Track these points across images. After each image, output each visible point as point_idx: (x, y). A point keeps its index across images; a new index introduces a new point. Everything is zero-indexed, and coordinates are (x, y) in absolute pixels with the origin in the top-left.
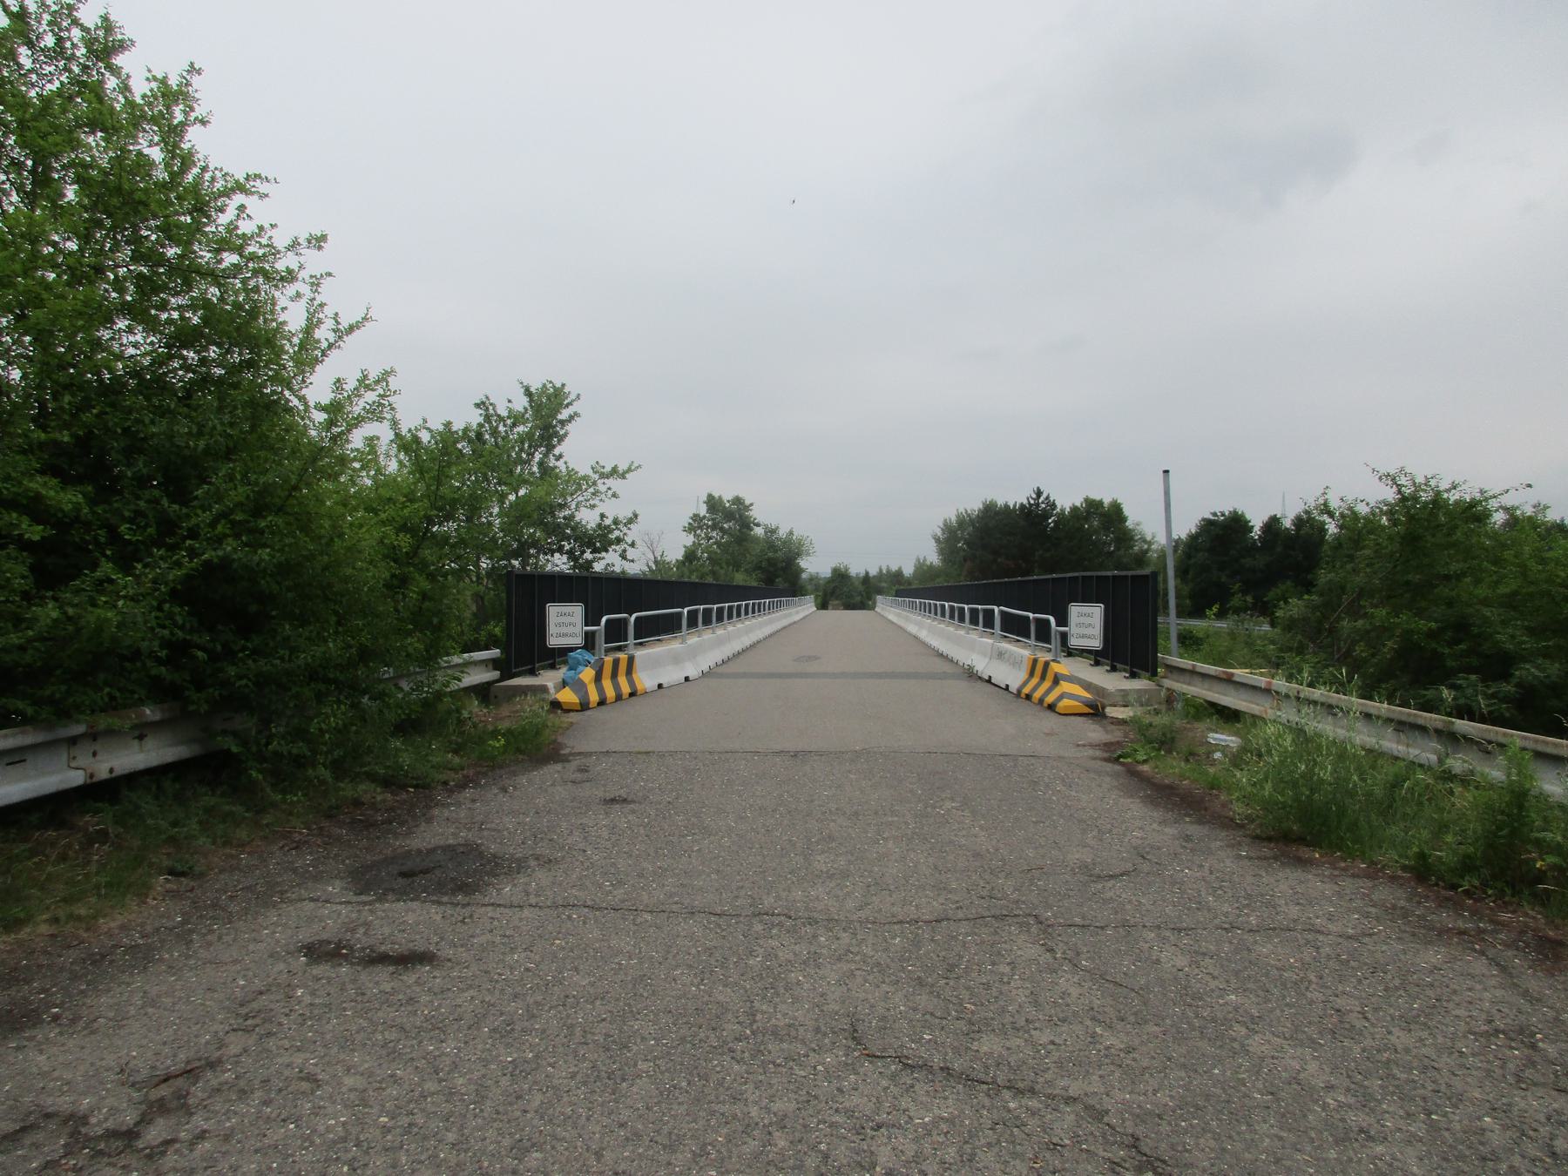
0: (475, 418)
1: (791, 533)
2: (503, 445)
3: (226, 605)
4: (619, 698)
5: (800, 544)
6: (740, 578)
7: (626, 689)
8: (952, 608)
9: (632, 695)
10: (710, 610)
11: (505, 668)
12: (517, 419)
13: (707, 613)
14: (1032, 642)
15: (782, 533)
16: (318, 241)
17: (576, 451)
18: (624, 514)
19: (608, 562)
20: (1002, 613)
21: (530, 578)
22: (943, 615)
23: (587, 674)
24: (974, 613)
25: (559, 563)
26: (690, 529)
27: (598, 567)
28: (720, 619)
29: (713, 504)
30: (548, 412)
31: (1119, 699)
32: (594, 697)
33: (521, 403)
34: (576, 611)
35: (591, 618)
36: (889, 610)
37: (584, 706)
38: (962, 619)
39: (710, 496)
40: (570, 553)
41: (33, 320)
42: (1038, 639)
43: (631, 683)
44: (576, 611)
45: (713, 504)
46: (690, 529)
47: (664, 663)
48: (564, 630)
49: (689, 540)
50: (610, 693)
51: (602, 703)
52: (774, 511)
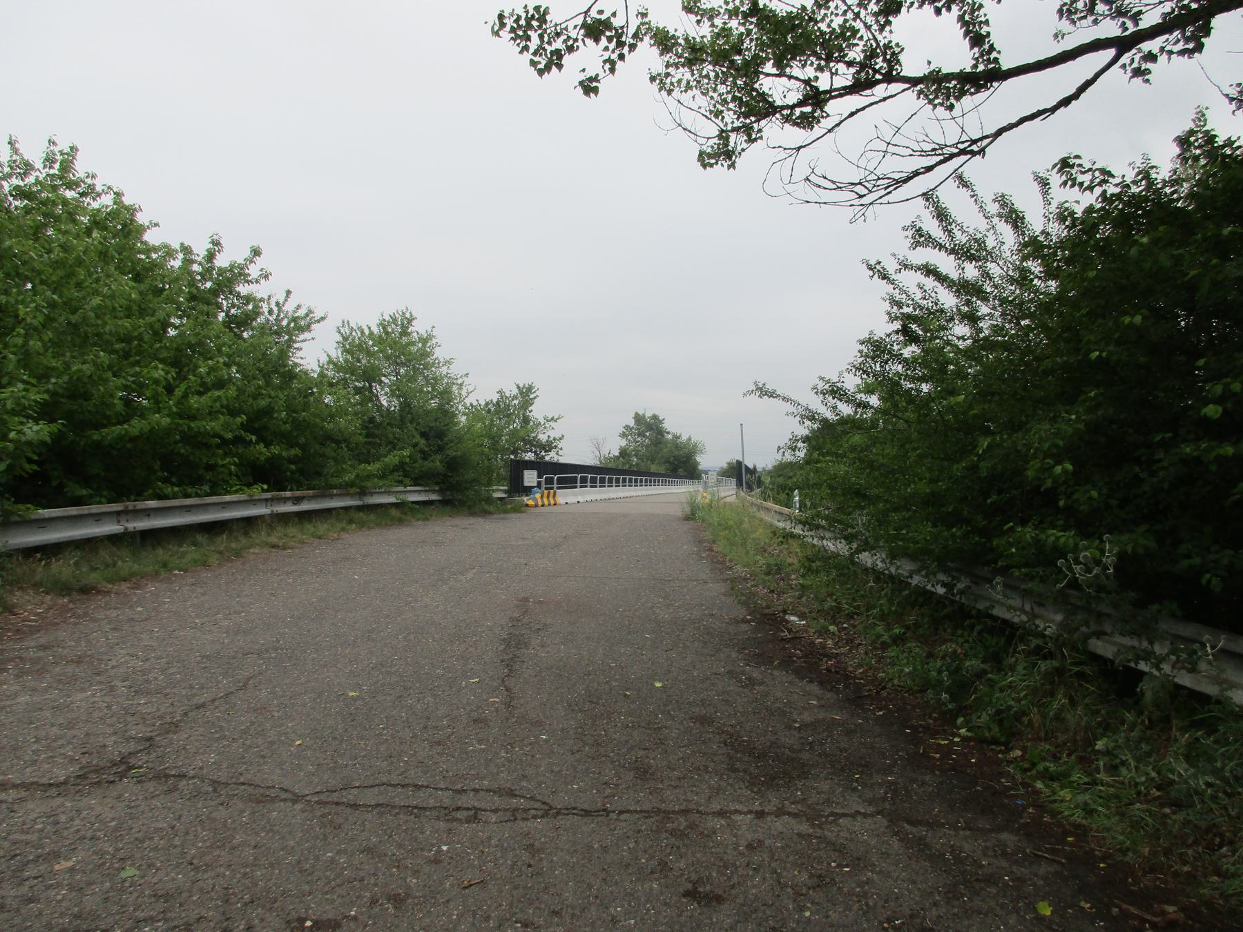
0: (495, 398)
1: (689, 439)
2: (508, 407)
3: (453, 465)
5: (695, 446)
6: (654, 468)
11: (509, 492)
12: (515, 397)
15: (684, 438)
17: (537, 412)
18: (558, 436)
19: (551, 457)
21: (518, 462)
23: (538, 496)
25: (530, 456)
26: (623, 435)
27: (547, 458)
29: (639, 419)
30: (526, 394)
32: (540, 503)
33: (515, 391)
34: (535, 473)
35: (540, 476)
37: (536, 506)
39: (637, 415)
40: (535, 453)
41: (1175, 732)
44: (535, 473)
45: (639, 419)
46: (623, 435)
47: (567, 497)
49: (624, 443)
52: (677, 426)
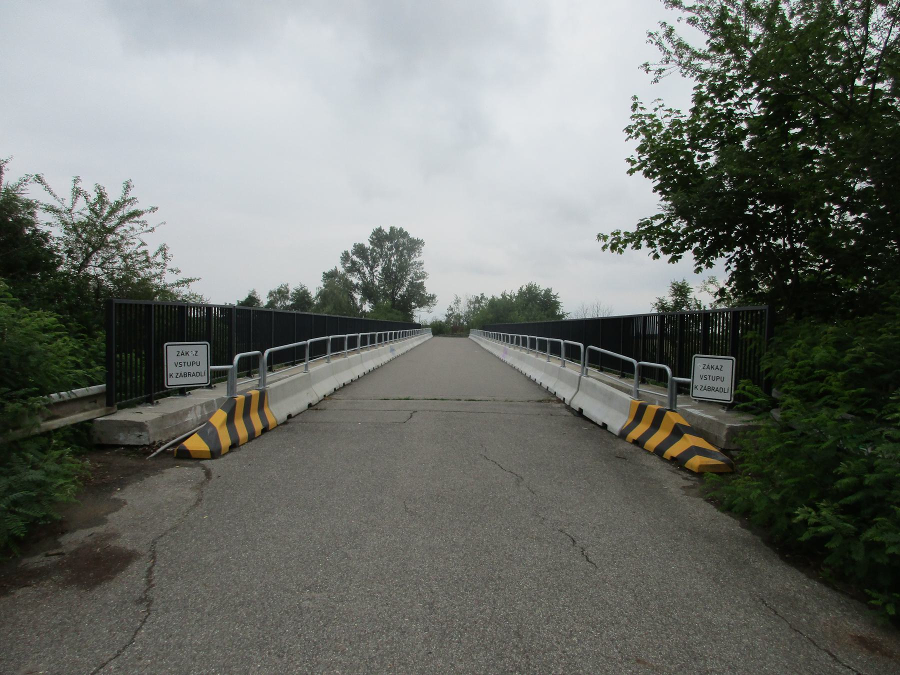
4: (252, 437)
7: (258, 426)
8: (512, 337)
9: (265, 430)
10: (374, 335)
13: (372, 337)
14: (548, 354)
16: (154, 209)
20: (566, 345)
22: (512, 342)
24: (533, 341)
28: (380, 340)
31: (209, 456)
32: (225, 441)
36: (475, 336)
38: (518, 343)
42: (540, 349)
43: (263, 417)
48: (709, 383)
50: (242, 432)
51: (234, 446)
